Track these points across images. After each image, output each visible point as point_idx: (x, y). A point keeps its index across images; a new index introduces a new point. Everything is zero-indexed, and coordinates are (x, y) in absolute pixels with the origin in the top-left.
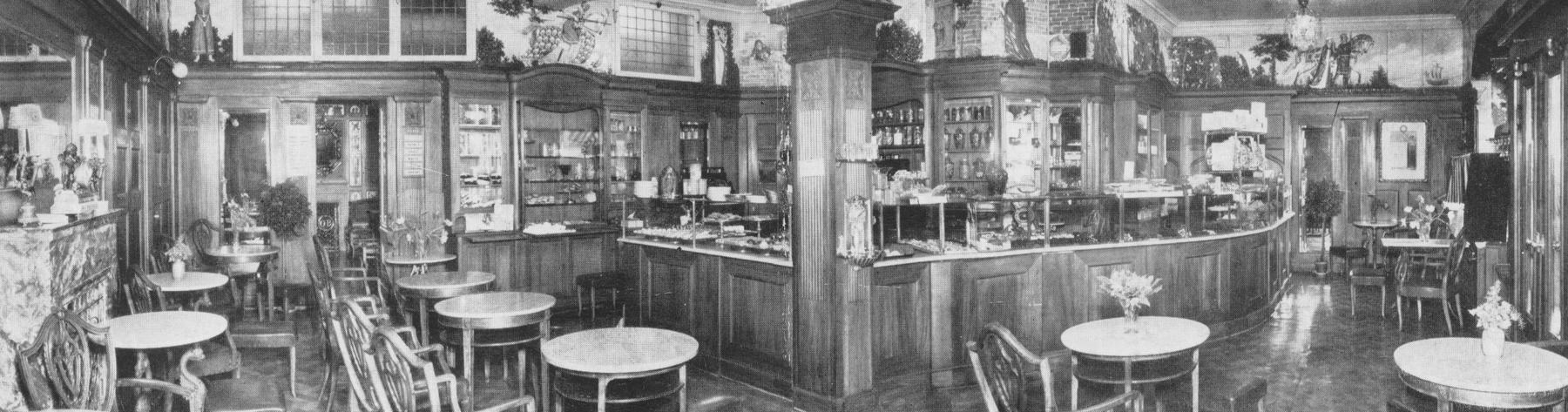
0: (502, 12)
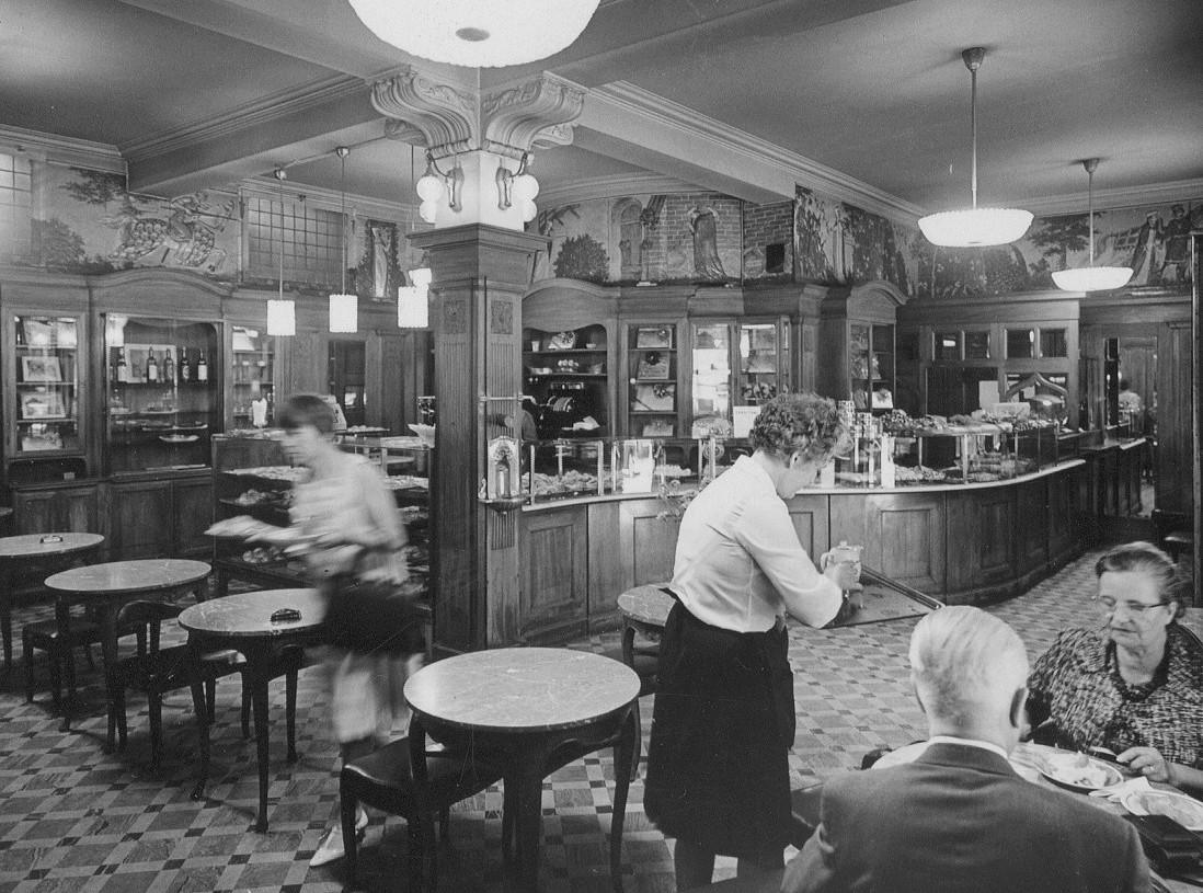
0: (81, 199)
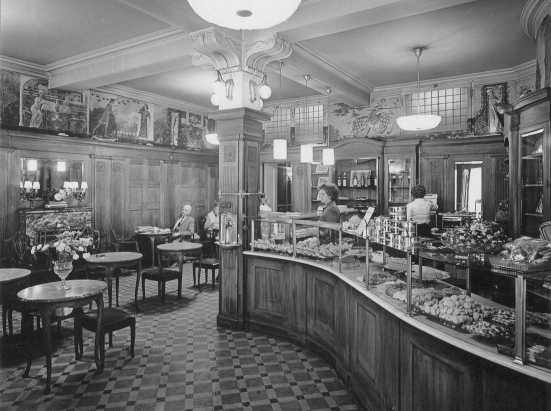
0: (338, 115)
